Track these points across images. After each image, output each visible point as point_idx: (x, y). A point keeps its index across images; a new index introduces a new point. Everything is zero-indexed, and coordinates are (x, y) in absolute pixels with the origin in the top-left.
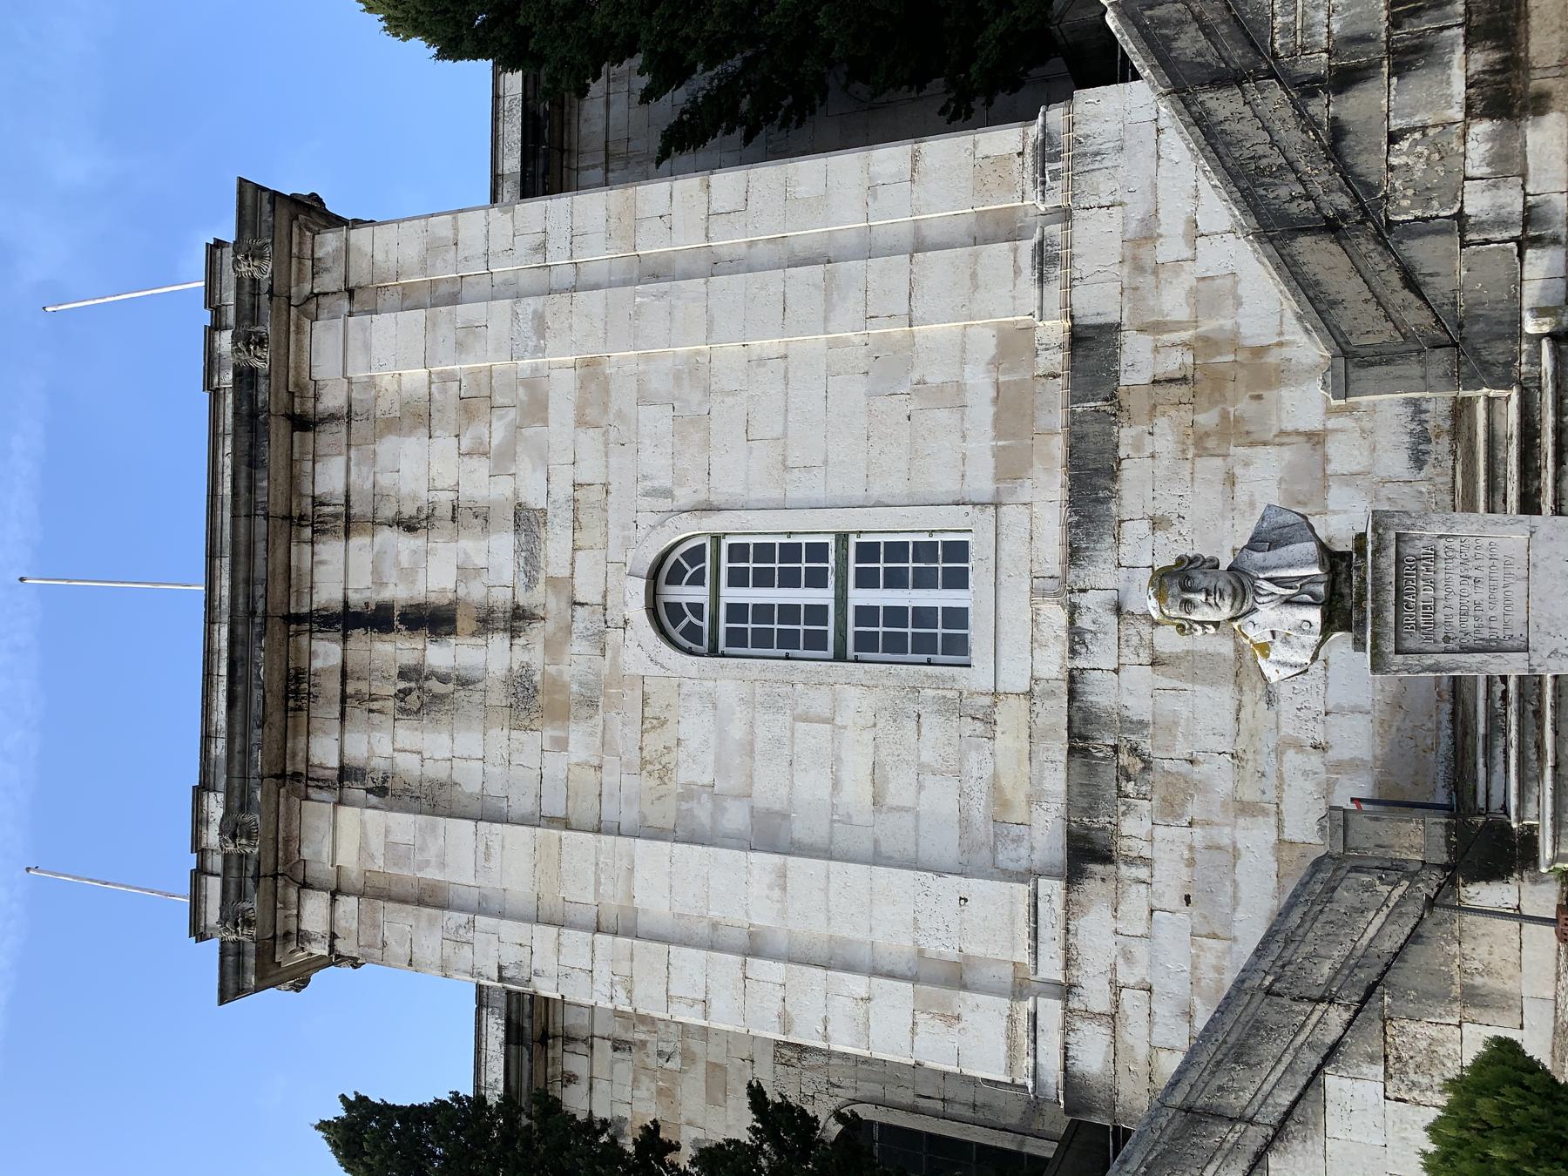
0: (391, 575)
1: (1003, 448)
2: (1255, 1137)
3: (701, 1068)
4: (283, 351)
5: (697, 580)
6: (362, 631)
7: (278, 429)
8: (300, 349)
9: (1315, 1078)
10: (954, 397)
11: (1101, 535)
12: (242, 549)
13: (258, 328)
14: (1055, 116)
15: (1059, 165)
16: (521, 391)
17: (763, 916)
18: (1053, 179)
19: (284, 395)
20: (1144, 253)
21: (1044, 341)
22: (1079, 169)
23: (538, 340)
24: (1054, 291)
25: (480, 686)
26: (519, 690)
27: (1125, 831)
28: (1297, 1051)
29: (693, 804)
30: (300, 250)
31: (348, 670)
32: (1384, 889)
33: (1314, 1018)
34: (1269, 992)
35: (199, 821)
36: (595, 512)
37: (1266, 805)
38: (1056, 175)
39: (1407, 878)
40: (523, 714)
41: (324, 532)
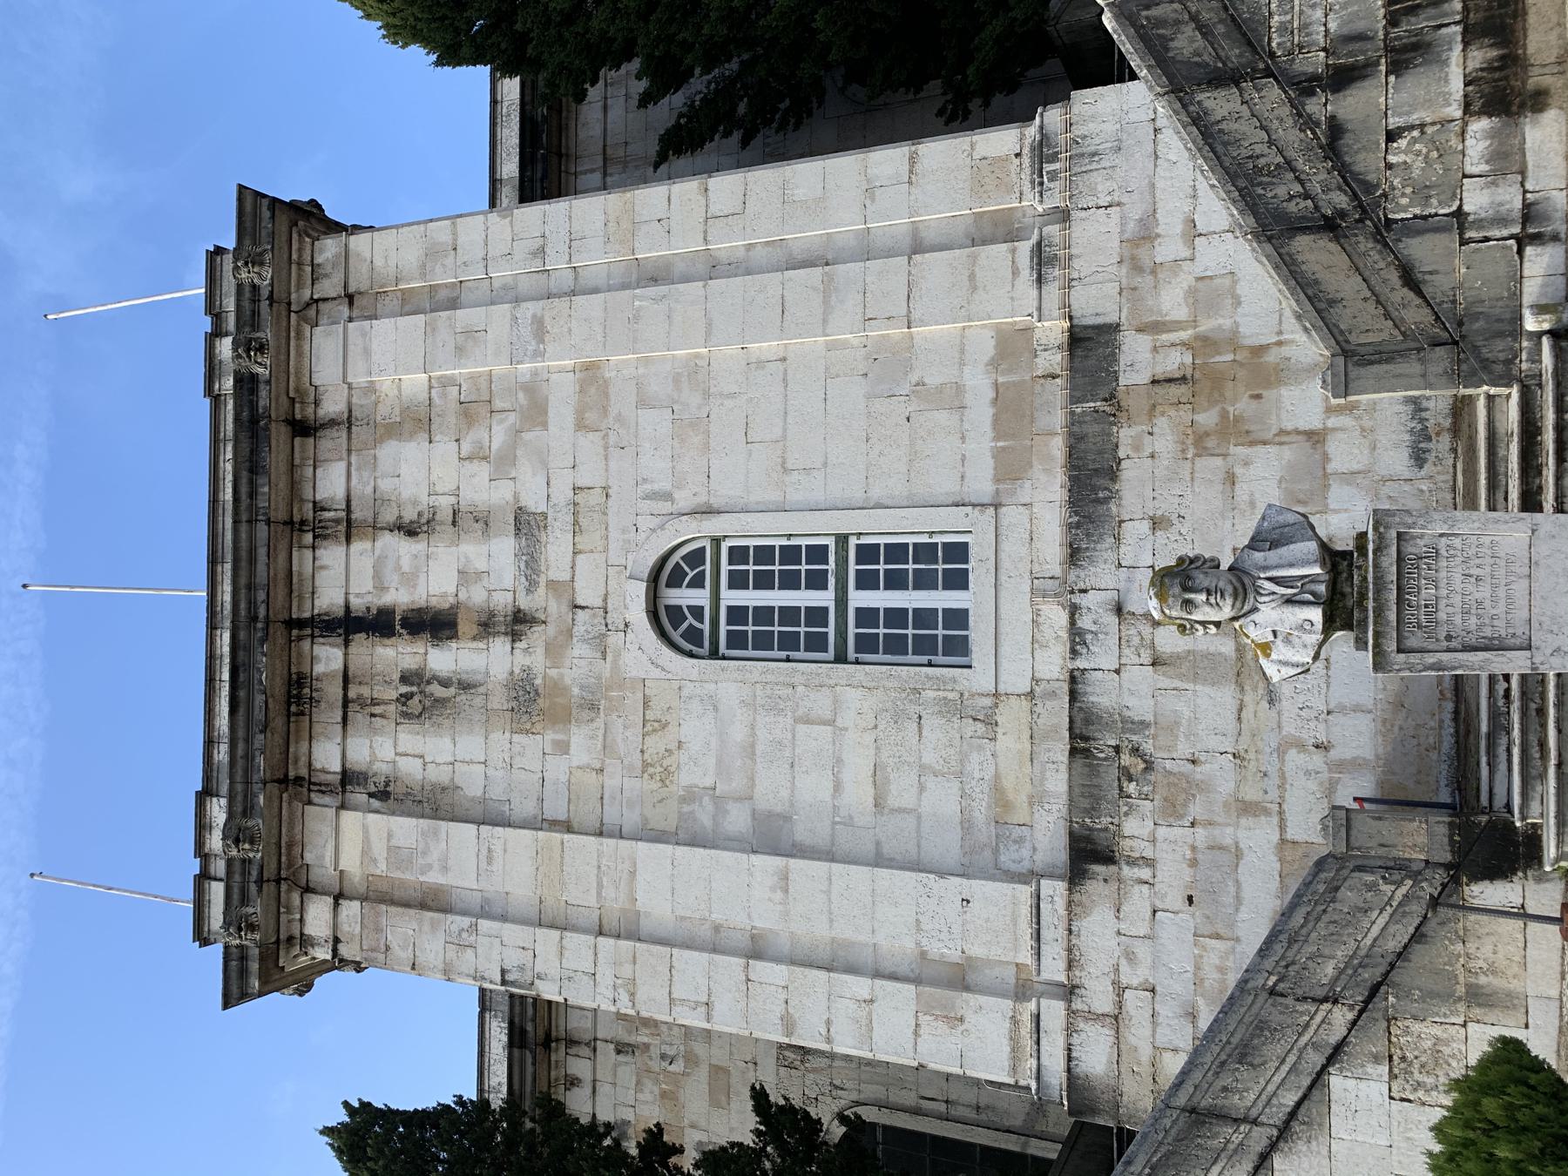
0: (392, 579)
2: (1259, 1138)
5: (698, 582)
6: (363, 635)
9: (1319, 1079)
10: (953, 398)
11: (1101, 535)
12: (244, 554)
14: (1052, 116)
15: (1057, 166)
16: (521, 395)
18: (1051, 180)
20: (1143, 253)
21: (1043, 342)
22: (1076, 169)
23: (538, 343)
24: (1052, 292)
25: (481, 690)
28: (1301, 1051)
29: (696, 806)
32: (1387, 889)
33: (1318, 1019)
34: (1272, 992)
35: (202, 826)
38: (1053, 176)
40: (525, 717)
41: (325, 537)
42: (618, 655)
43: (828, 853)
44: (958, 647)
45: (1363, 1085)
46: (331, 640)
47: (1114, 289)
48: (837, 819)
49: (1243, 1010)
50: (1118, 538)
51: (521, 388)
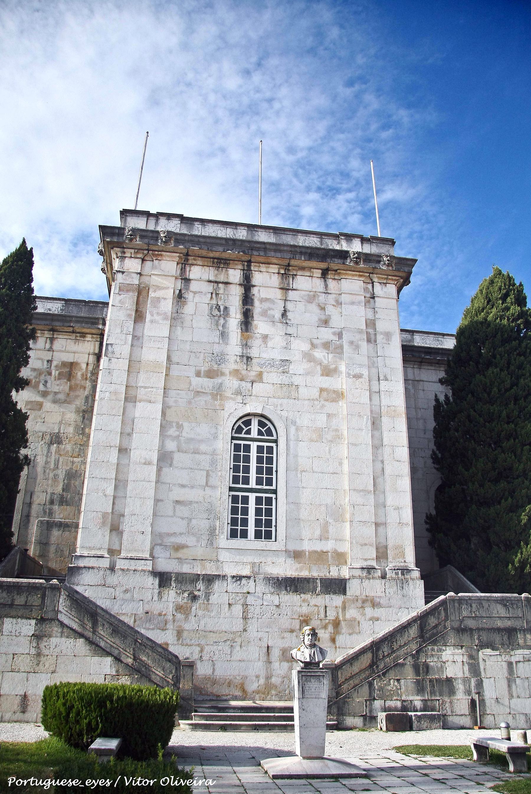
0: (266, 305)
1: (305, 554)
2: (89, 634)
3: (39, 399)
4: (353, 269)
5: (260, 433)
6: (243, 292)
7: (324, 265)
8: (353, 275)
9: (109, 654)
10: (324, 537)
11: (274, 588)
12: (279, 247)
13: (362, 261)
14: (416, 574)
15: (400, 575)
16: (334, 366)
17: (136, 455)
18: (396, 573)
19: (336, 268)
20: (368, 604)
21: (342, 569)
22: (398, 581)
23: (353, 375)
24: (358, 573)
25: (221, 342)
26: (220, 358)
27: (171, 592)
28: (117, 649)
29: (175, 429)
30: (390, 279)
31: (228, 285)
32: (171, 676)
33: (128, 654)
34: (136, 641)
35: (169, 216)
36: (287, 393)
37: (181, 640)
38: (397, 574)
39: (174, 682)
40: (210, 359)
41: (282, 279)
42: (234, 399)
43: (158, 481)
44: (233, 534)
45: (109, 667)
46: (242, 277)
47: (358, 593)
48: (171, 485)
49: (129, 631)
50: (272, 593)
51: (337, 366)
